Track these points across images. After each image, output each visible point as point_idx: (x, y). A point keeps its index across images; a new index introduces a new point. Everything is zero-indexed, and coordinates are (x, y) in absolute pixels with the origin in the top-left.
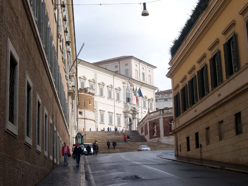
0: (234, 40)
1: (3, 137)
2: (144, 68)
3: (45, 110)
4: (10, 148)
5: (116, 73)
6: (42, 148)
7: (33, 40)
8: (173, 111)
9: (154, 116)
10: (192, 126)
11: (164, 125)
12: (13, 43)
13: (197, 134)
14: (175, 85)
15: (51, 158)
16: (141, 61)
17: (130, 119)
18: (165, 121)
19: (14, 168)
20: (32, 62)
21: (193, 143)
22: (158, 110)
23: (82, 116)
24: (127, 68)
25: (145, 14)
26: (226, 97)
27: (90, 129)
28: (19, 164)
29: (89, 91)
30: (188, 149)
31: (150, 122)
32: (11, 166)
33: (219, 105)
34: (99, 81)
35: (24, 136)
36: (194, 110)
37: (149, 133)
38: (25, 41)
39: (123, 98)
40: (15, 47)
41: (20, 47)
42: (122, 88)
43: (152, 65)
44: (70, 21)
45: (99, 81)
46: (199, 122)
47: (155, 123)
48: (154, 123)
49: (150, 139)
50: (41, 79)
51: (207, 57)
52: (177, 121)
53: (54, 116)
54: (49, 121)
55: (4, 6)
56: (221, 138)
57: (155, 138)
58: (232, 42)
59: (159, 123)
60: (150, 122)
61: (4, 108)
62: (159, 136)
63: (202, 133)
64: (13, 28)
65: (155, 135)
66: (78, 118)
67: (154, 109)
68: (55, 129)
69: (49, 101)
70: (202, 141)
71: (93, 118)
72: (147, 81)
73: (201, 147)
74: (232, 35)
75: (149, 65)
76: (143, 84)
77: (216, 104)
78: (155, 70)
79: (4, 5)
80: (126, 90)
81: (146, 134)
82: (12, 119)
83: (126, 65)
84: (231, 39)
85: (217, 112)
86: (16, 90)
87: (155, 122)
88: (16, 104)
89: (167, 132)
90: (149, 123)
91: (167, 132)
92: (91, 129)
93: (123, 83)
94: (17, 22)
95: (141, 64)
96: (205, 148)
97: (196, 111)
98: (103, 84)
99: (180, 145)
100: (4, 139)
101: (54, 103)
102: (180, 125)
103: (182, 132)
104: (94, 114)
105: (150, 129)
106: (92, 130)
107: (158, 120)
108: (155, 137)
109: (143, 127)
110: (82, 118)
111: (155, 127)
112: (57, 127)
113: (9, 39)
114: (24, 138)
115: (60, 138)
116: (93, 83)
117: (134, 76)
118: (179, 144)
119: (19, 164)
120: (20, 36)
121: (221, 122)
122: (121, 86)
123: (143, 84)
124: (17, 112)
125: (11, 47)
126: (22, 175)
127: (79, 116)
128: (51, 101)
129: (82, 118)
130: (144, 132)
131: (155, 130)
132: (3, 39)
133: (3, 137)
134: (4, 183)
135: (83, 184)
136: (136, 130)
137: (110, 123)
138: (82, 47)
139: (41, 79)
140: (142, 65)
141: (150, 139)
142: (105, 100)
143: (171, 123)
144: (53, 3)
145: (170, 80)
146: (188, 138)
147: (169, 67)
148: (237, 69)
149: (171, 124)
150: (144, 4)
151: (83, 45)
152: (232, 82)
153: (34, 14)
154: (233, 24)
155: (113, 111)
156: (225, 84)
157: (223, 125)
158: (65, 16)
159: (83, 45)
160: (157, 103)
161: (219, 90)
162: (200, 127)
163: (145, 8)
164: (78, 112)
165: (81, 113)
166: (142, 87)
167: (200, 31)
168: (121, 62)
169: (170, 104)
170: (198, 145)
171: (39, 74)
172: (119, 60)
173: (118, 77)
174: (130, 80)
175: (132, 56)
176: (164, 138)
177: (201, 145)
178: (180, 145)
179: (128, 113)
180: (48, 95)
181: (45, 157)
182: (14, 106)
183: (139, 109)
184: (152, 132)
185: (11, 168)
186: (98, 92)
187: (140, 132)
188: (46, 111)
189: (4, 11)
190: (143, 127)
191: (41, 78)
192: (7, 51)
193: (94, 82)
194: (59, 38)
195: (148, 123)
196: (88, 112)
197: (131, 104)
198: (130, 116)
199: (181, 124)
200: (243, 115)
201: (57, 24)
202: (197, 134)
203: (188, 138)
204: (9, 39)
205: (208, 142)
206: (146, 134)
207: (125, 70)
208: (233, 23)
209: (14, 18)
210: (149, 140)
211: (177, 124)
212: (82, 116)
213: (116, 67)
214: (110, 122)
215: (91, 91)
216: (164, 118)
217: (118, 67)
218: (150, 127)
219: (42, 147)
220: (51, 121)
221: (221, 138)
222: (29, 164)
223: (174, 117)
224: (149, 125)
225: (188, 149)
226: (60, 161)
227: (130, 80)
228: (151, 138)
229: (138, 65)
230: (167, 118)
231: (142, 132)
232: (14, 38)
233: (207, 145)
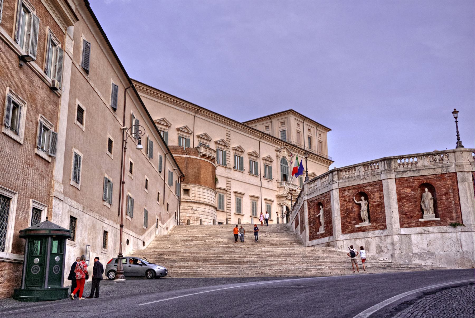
11: (342, 206)
16: (305, 118)
17: (287, 208)
18: (343, 197)
23: (189, 198)
31: (310, 202)
37: (307, 228)
39: (277, 174)
42: (274, 158)
47: (320, 204)
59: (329, 201)
60: (310, 202)
65: (322, 230)
66: (181, 200)
72: (315, 149)
75: (318, 125)
76: (307, 153)
78: (329, 133)
80: (281, 162)
87: (322, 201)
89: (350, 223)
90: (309, 205)
95: (305, 123)
104: (214, 195)
105: (309, 218)
107: (328, 194)
108: (322, 236)
110: (187, 202)
111: (321, 213)
116: (223, 147)
127: (183, 196)
129: (187, 202)
131: (322, 220)
140: (305, 127)
142: (246, 177)
143: (361, 202)
155: (258, 195)
164: (182, 190)
165: (187, 191)
173: (265, 139)
175: (291, 110)
176: (342, 237)
193: (224, 146)
195: (306, 204)
196: (201, 190)
197: (289, 184)
207: (279, 132)
212: (189, 198)
213: (266, 129)
214: (253, 212)
216: (342, 190)
217: (270, 127)
218: (309, 212)
224: (309, 209)
228: (312, 238)
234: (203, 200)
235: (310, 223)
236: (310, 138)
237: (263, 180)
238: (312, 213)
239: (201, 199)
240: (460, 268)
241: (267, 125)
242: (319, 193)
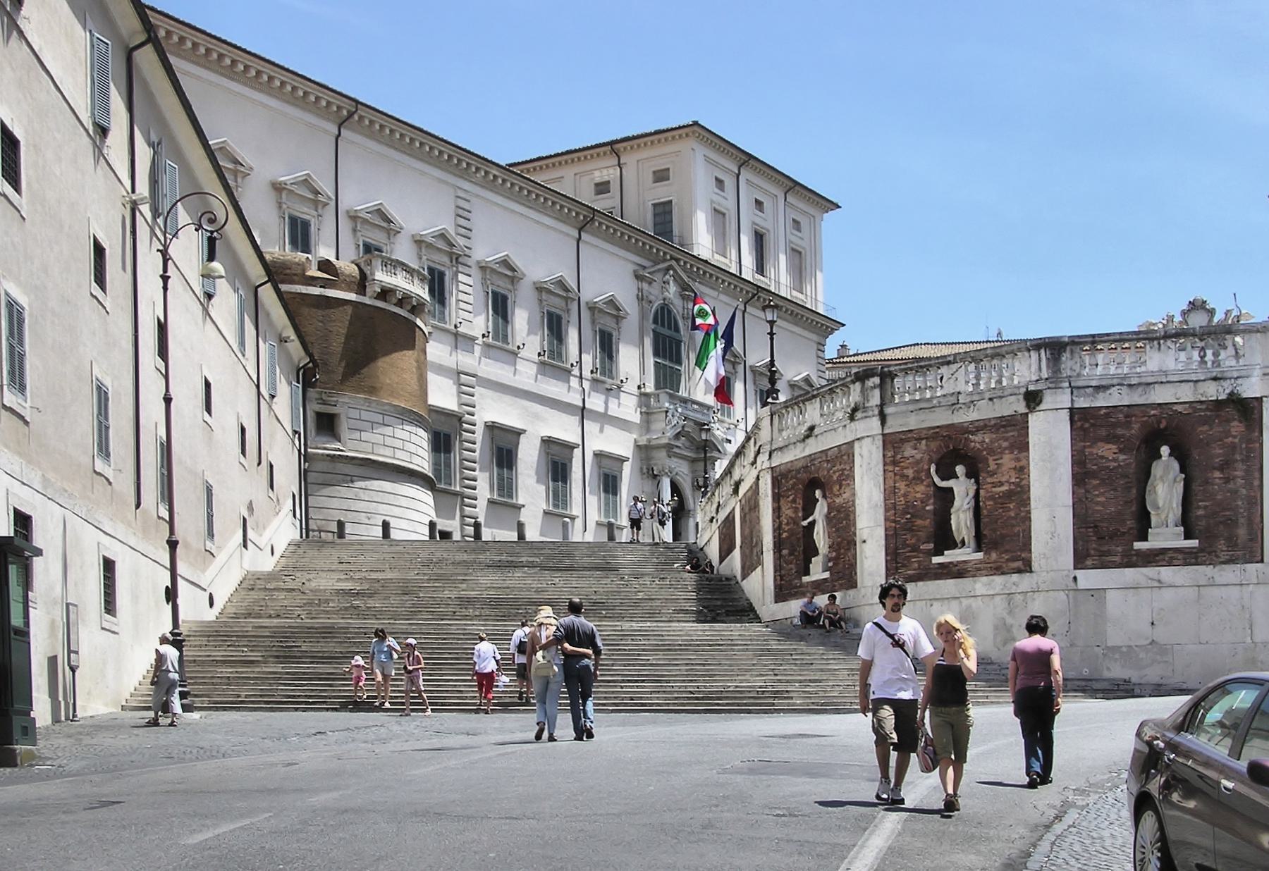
2: (767, 205)
16: (747, 160)
18: (895, 463)
24: (661, 193)
27: (386, 526)
43: (811, 191)
47: (814, 483)
57: (851, 543)
59: (847, 477)
60: (779, 478)
65: (817, 572)
71: (417, 460)
75: (792, 186)
80: (655, 321)
81: (750, 564)
83: (661, 176)
87: (822, 474)
89: (915, 549)
90: (776, 482)
91: (915, 549)
92: (393, 523)
105: (777, 530)
106: (394, 534)
107: (845, 454)
109: (729, 520)
111: (821, 510)
130: (737, 553)
131: (821, 538)
135: (1227, 363)
137: (556, 506)
149: (951, 490)
166: (749, 309)
174: (677, 260)
184: (795, 549)
190: (729, 520)
196: (405, 435)
198: (682, 470)
210: (769, 608)
216: (892, 443)
217: (615, 187)
218: (777, 511)
224: (776, 498)
227: (677, 260)
228: (782, 594)
229: (729, 183)
230: (919, 439)
231: (726, 550)
233: (16, 512)
235: (778, 545)
238: (787, 512)
239: (399, 454)
241: (599, 176)
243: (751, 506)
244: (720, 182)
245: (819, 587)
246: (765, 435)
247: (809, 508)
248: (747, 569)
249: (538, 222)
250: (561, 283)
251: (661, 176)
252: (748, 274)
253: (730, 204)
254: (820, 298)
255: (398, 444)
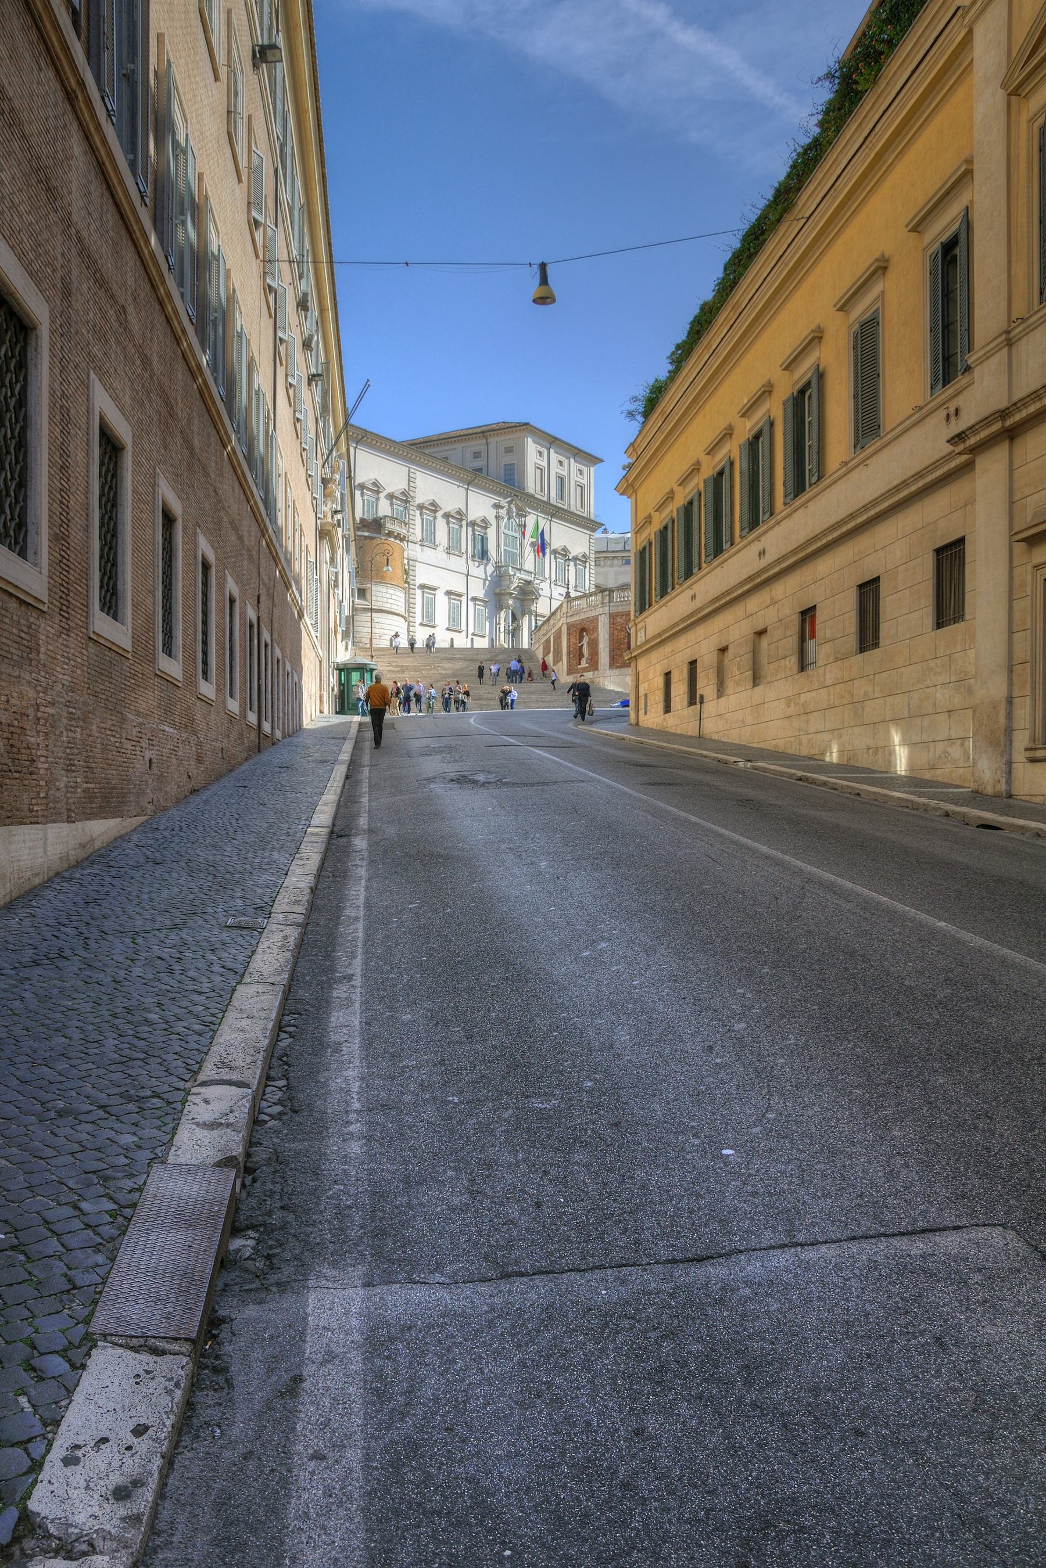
0: (813, 390)
1: (81, 653)
3: (229, 579)
4: (107, 684)
5: (474, 476)
6: (219, 690)
7: (183, 373)
8: (631, 596)
9: (584, 610)
10: (682, 641)
11: (611, 635)
12: (108, 388)
13: (693, 664)
14: (641, 516)
15: (252, 718)
19: (120, 738)
20: (179, 440)
21: (679, 690)
22: (600, 590)
24: (507, 459)
25: (544, 299)
26: (778, 561)
28: (138, 729)
29: (389, 526)
30: (667, 709)
32: (108, 732)
33: (760, 583)
34: (421, 497)
35: (154, 655)
36: (689, 593)
37: (565, 658)
38: (151, 378)
40: (116, 399)
41: (133, 399)
43: (590, 455)
44: (322, 311)
45: (421, 497)
46: (700, 631)
47: (583, 630)
48: (582, 630)
49: (568, 674)
50: (215, 491)
51: (734, 436)
52: (642, 624)
53: (261, 600)
54: (243, 614)
55: (73, 278)
56: (756, 679)
58: (810, 397)
60: (570, 627)
61: (84, 575)
62: (594, 665)
63: (707, 658)
64: (106, 341)
65: (584, 664)
67: (589, 586)
68: (266, 636)
69: (246, 557)
70: (706, 686)
73: (702, 702)
74: (809, 375)
77: (750, 578)
79: (75, 272)
81: (557, 659)
82: (111, 604)
84: (808, 385)
85: (753, 603)
86: (123, 524)
88: (124, 563)
90: (569, 629)
93: (497, 506)
94: (124, 324)
96: (711, 707)
97: (693, 597)
98: (434, 508)
99: (646, 695)
100: (85, 658)
101: (262, 561)
102: (649, 636)
103: (654, 656)
105: (569, 647)
107: (595, 619)
108: (585, 670)
109: (548, 641)
112: (275, 633)
113: (93, 376)
114: (154, 659)
115: (284, 664)
117: (531, 485)
118: (642, 692)
119: (138, 729)
120: (134, 363)
121: (761, 633)
122: (490, 514)
123: (555, 512)
124: (129, 586)
125: (102, 401)
126: (147, 759)
128: (251, 556)
130: (551, 654)
132: (73, 376)
133: (81, 653)
134: (86, 777)
136: (526, 646)
138: (361, 397)
139: (215, 491)
141: (568, 674)
142: (439, 556)
144: (257, 257)
145: (626, 504)
146: (668, 675)
147: (626, 463)
148: (814, 479)
150: (543, 267)
151: (367, 386)
152: (799, 516)
153: (182, 295)
154: (817, 337)
156: (778, 523)
157: (765, 642)
158: (305, 295)
159: (367, 386)
160: (599, 569)
161: (763, 539)
162: (701, 644)
163: (544, 280)
167: (719, 357)
168: (493, 440)
169: (628, 575)
170: (693, 697)
171: (207, 475)
172: (485, 433)
177: (702, 697)
178: (646, 695)
179: (507, 597)
180: (240, 538)
181: (231, 718)
182: (120, 569)
183: (542, 586)
185: (112, 739)
186: (417, 531)
187: (540, 654)
188: (232, 586)
189: (74, 291)
190: (548, 641)
191: (215, 487)
192: (89, 411)
194: (281, 364)
199: (650, 633)
200: (820, 616)
201: (272, 320)
202: (693, 664)
203: (668, 675)
204: (93, 376)
205: (721, 691)
206: (557, 659)
208: (817, 334)
209: (112, 312)
211: (639, 635)
215: (397, 528)
217: (484, 455)
218: (569, 640)
219: (218, 685)
220: (251, 614)
221: (756, 679)
222: (172, 730)
223: (632, 614)
224: (569, 634)
225: (667, 709)
226: (284, 728)
228: (570, 672)
232: (112, 370)
234: (388, 605)
235: (569, 653)
236: (561, 479)
237: (469, 561)
238: (573, 640)
239: (393, 606)
240: (619, 690)
241: (476, 449)
242: (583, 616)
243: (558, 636)
244: (540, 453)
245: (585, 670)
246: (564, 609)
247: (581, 640)
248: (556, 662)
249: (310, 29)
250: (459, 512)
251: (509, 450)
252: (553, 501)
253: (545, 464)
254: (592, 511)
255: (389, 596)
